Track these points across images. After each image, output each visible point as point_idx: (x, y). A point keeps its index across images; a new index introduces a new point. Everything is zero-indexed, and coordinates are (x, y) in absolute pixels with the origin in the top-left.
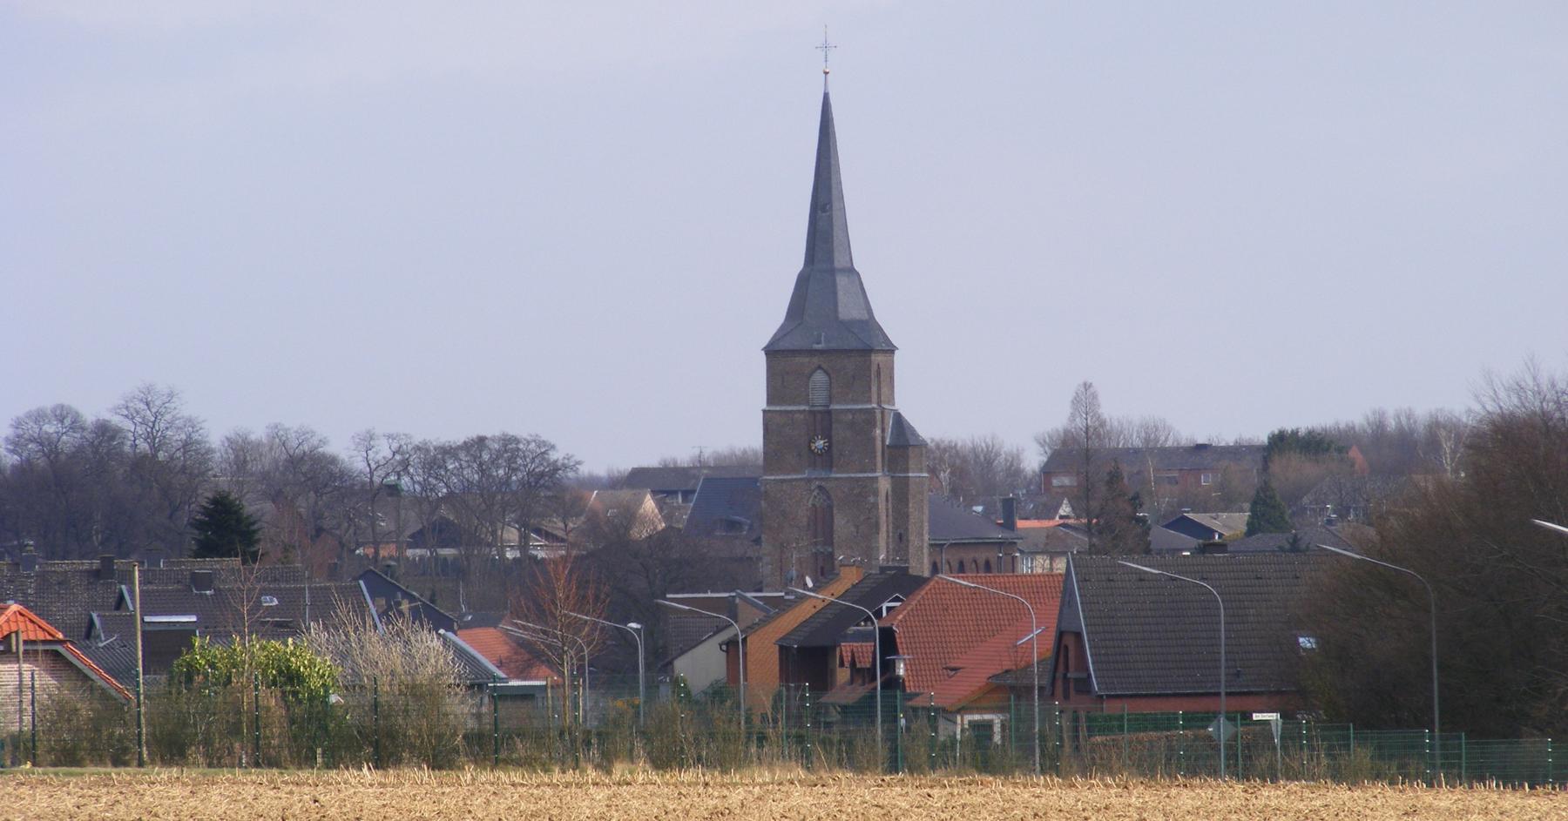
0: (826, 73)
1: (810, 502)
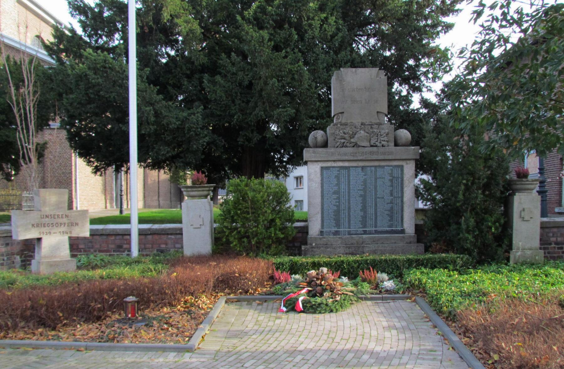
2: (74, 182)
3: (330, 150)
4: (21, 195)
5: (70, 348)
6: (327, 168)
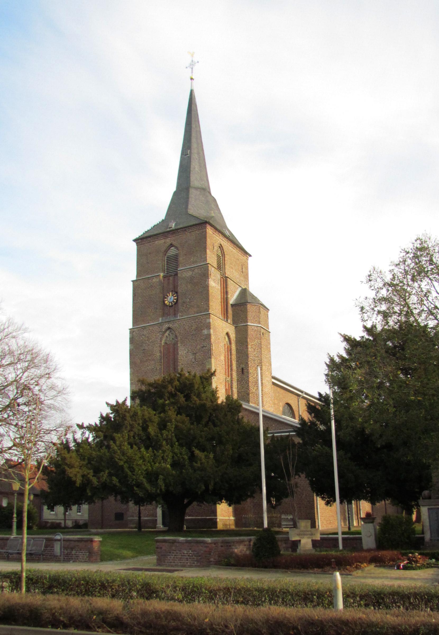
0: (192, 79)
1: (163, 342)
2: (316, 508)
3: (432, 500)
4: (280, 517)
5: (312, 573)
6: (432, 509)
